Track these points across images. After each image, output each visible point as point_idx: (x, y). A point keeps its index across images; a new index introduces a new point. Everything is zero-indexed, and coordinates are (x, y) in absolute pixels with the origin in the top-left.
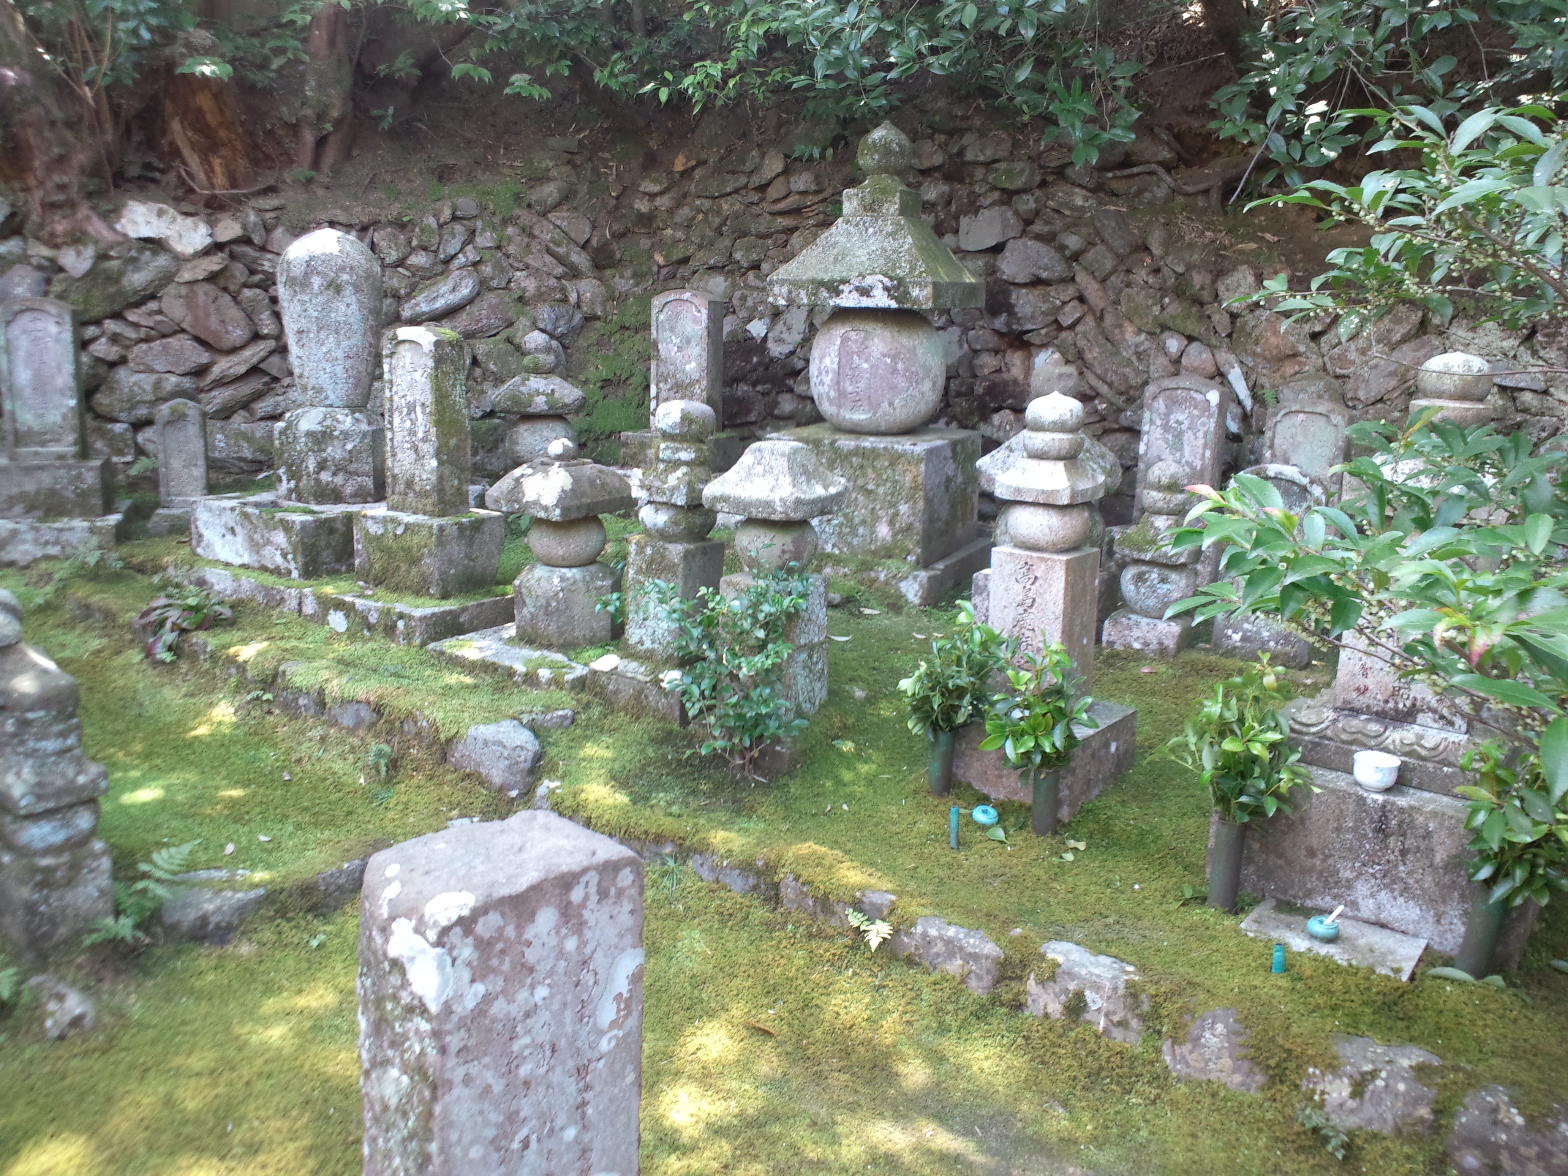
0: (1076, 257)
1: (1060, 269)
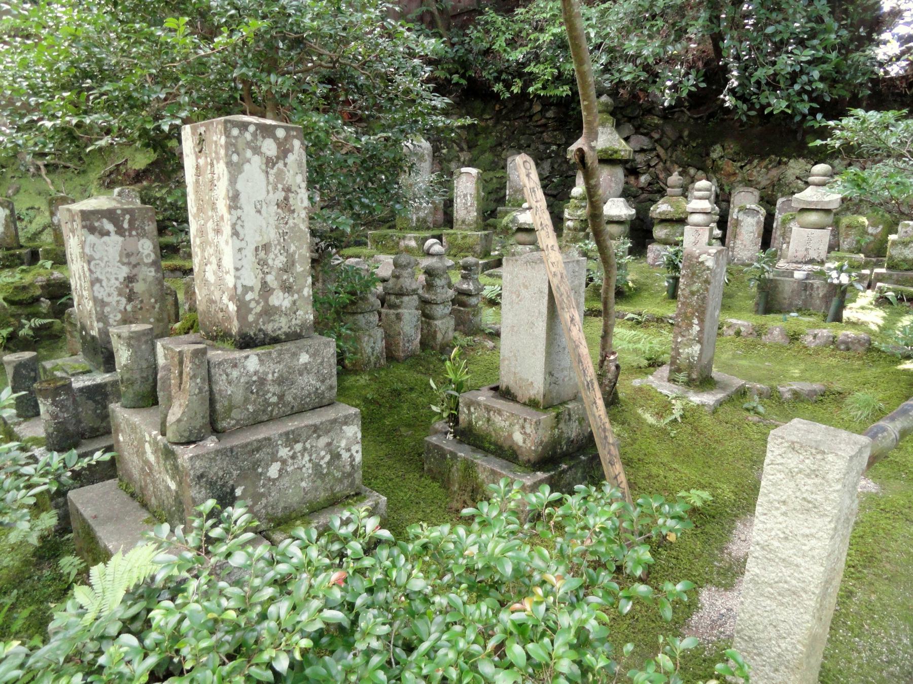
0: (656, 141)
1: (650, 146)
